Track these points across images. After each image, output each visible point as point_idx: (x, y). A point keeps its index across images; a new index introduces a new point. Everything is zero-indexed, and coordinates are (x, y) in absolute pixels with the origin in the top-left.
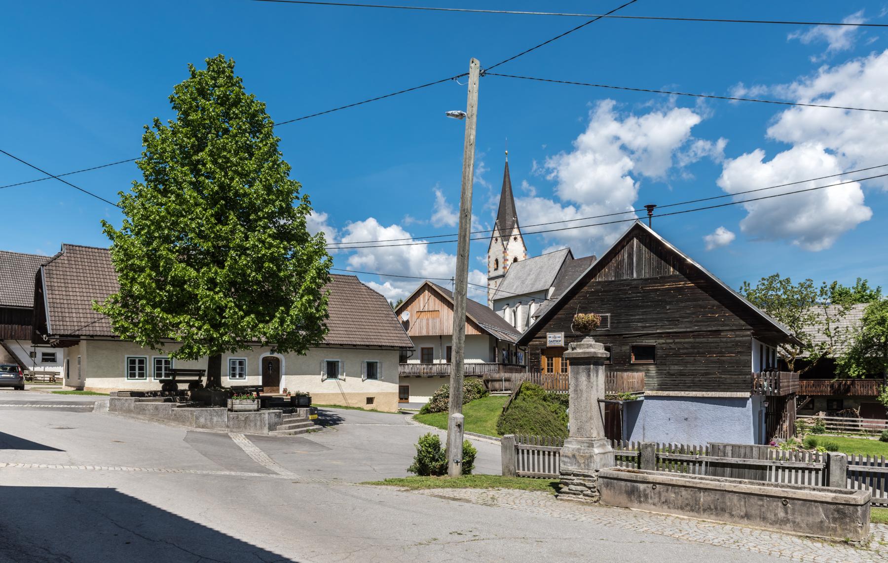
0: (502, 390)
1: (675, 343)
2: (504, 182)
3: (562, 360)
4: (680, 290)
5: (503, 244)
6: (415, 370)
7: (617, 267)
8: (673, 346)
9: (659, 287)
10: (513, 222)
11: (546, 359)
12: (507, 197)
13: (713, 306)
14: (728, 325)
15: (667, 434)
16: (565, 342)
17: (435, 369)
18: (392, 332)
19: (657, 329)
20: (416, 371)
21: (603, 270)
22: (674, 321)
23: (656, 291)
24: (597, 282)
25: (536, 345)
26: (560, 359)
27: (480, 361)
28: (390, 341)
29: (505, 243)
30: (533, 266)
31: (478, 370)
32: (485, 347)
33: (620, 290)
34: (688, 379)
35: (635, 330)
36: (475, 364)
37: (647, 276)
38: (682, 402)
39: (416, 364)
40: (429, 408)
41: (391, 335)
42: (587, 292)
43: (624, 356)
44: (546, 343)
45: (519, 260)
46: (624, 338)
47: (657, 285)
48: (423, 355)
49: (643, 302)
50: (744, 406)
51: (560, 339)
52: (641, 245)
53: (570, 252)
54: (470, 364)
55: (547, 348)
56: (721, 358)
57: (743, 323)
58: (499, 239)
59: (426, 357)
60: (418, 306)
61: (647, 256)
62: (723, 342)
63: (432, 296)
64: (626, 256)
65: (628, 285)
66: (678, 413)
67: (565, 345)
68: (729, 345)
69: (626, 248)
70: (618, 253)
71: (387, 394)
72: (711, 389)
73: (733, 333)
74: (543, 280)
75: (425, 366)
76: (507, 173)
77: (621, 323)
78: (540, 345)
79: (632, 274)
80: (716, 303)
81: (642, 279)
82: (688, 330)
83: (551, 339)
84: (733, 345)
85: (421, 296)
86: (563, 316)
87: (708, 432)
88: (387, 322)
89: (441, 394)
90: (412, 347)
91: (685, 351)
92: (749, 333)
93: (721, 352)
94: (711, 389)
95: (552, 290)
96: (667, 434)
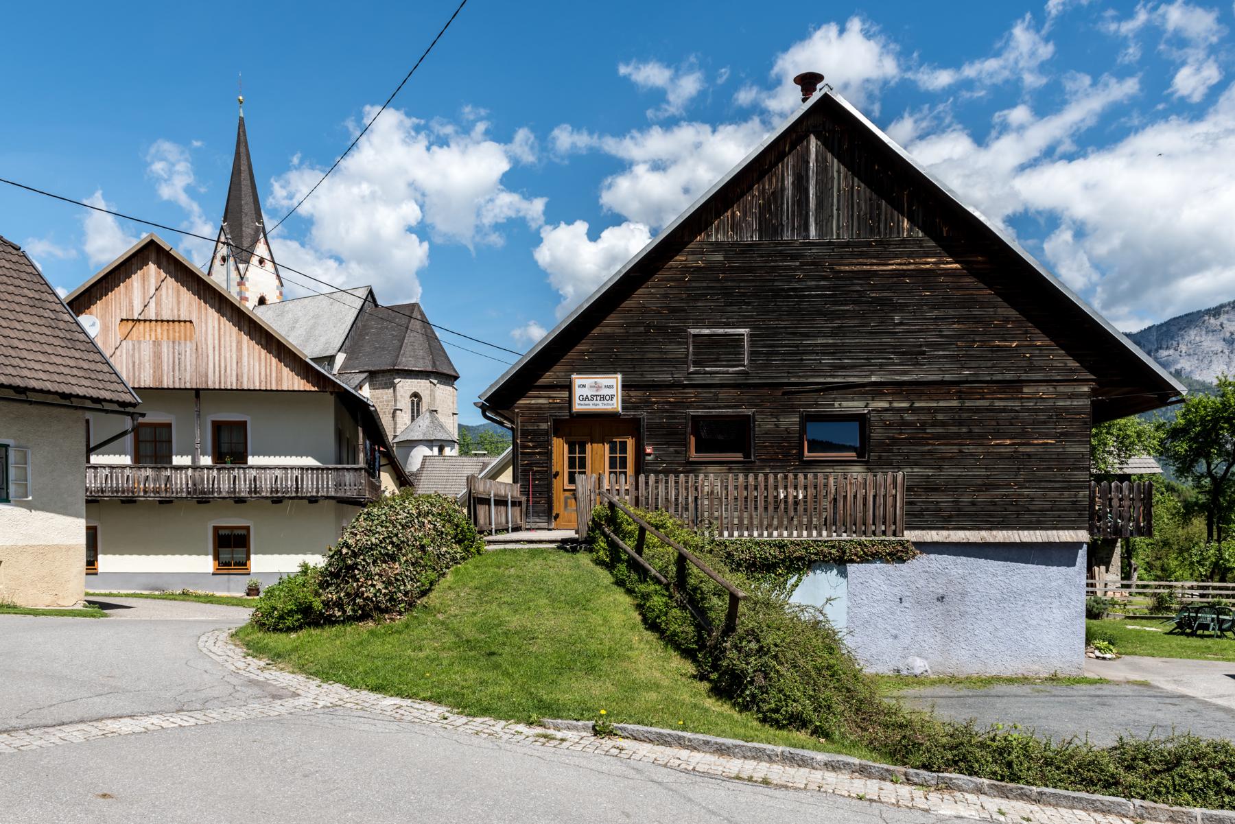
0: (490, 534)
1: (912, 409)
2: (238, 154)
3: (612, 450)
4: (926, 277)
5: (238, 269)
6: (119, 481)
7: (764, 209)
8: (908, 417)
9: (875, 268)
10: (257, 231)
11: (566, 447)
12: (244, 183)
13: (1007, 320)
14: (1041, 369)
15: (896, 637)
16: (623, 401)
17: (180, 481)
18: (60, 351)
19: (872, 372)
20: (122, 483)
21: (729, 213)
22: (914, 355)
23: (869, 278)
24: (712, 243)
25: (540, 407)
26: (607, 446)
27: (310, 461)
28: (55, 377)
29: (242, 267)
30: (300, 314)
31: (309, 486)
32: (324, 424)
33: (774, 268)
34: (944, 499)
35: (816, 372)
36: (302, 468)
37: (846, 237)
38: (932, 556)
39: (123, 467)
40: (317, 604)
41: (59, 360)
42: (686, 269)
43: (785, 441)
44: (570, 400)
45: (268, 302)
46: (784, 394)
47: (869, 261)
48: (137, 443)
49: (835, 303)
50: (1071, 563)
51: (613, 392)
52: (829, 156)
53: (371, 293)
54: (285, 468)
55: (571, 415)
56: (1022, 449)
57: (1073, 364)
58: (231, 261)
59: (147, 449)
60: (125, 303)
61: (843, 184)
62: (1028, 410)
63: (171, 281)
64: (789, 181)
65: (794, 257)
66: (921, 583)
67: (623, 408)
68: (1042, 417)
69: (790, 161)
70: (770, 170)
71: (42, 552)
72: (999, 523)
73: (1051, 389)
74: (323, 340)
75: (149, 472)
76: (242, 138)
77: (778, 353)
78: (551, 407)
79: (807, 229)
80: (1013, 313)
81: (830, 243)
82: (948, 377)
83: (587, 392)
84: (1051, 417)
85: (136, 279)
86: (617, 330)
87: (991, 629)
88: (36, 320)
89: (373, 547)
90: (134, 405)
91: (939, 430)
92: (1086, 389)
93: (1023, 434)
94: (999, 523)
95: (340, 359)
96: (896, 637)
